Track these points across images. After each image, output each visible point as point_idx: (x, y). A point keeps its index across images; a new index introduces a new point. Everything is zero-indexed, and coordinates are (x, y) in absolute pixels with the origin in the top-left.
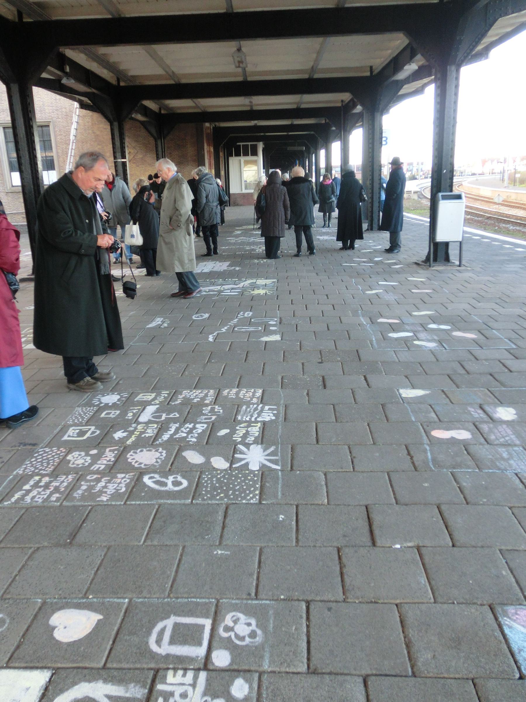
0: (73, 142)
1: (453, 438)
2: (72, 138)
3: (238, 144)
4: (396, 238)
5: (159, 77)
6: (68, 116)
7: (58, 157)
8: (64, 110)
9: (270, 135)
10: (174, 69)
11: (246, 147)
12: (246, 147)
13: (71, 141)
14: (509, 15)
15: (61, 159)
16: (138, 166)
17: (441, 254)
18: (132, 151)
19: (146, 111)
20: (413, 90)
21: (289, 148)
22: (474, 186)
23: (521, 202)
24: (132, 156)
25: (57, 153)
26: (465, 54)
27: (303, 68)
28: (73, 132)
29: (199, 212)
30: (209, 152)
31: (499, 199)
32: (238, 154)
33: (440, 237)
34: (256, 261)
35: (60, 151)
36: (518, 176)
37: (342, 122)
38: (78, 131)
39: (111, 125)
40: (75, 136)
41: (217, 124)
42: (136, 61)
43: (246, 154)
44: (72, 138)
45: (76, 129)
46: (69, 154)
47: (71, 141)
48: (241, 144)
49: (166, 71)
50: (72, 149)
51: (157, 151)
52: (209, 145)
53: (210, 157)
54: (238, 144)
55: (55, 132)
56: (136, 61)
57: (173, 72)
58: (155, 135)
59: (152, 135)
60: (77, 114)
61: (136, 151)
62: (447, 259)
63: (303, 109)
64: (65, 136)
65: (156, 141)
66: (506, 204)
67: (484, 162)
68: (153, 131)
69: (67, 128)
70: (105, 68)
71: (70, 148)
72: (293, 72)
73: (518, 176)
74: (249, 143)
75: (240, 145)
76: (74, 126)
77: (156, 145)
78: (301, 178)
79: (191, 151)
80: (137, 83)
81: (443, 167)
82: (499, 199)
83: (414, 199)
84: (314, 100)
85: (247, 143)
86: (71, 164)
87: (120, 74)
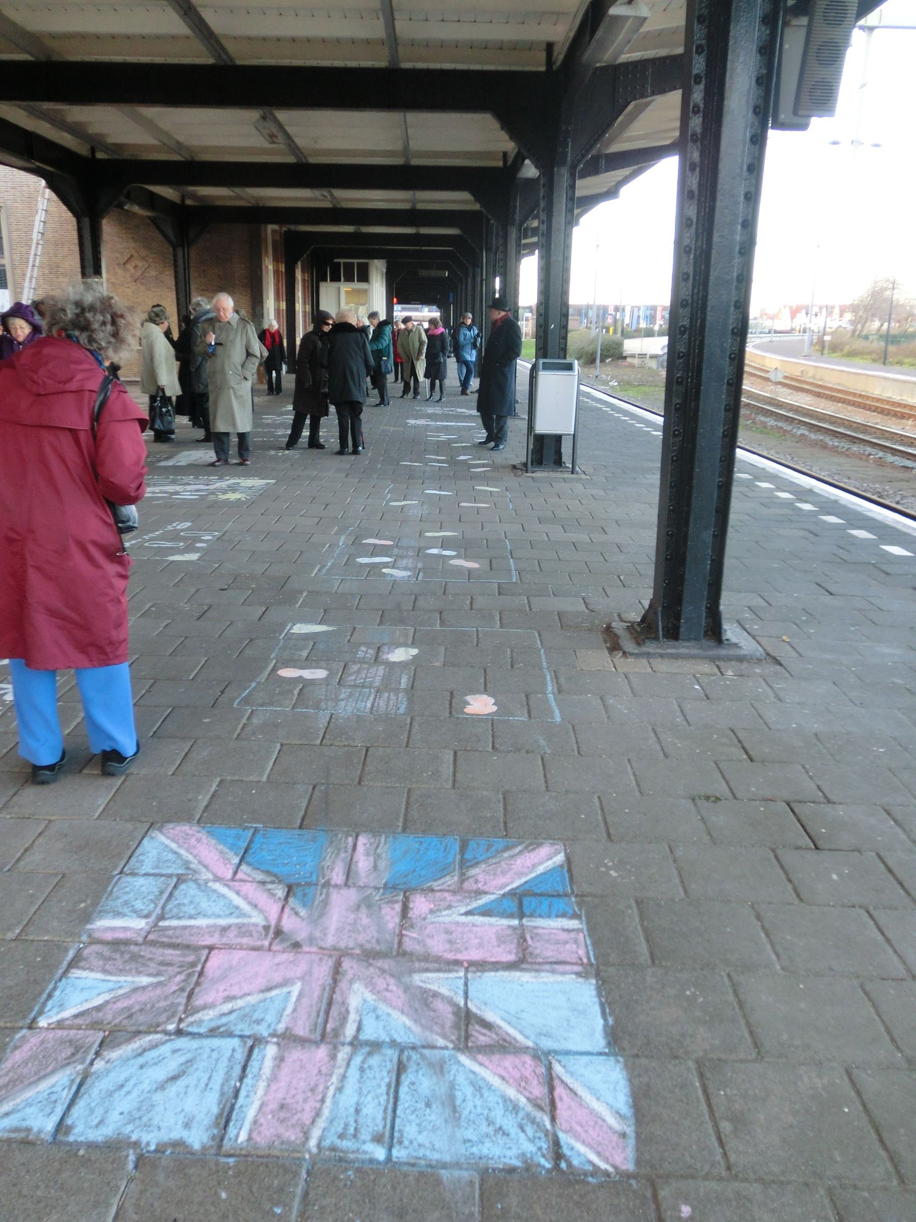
0: (38, 244)
1: (301, 677)
2: (35, 236)
3: (336, 260)
4: (503, 427)
5: (153, 148)
6: (31, 200)
7: (13, 266)
8: (25, 188)
9: (392, 250)
10: (181, 138)
11: (349, 268)
12: (349, 268)
13: (35, 242)
14: (647, 97)
15: (18, 271)
16: (149, 289)
17: (549, 453)
18: (140, 264)
19: (152, 201)
20: (605, 190)
21: (423, 273)
22: (759, 352)
23: (820, 383)
24: (139, 273)
25: (12, 260)
26: (583, 152)
27: (391, 148)
28: (38, 226)
29: (193, 370)
30: (276, 272)
31: (776, 375)
32: (336, 278)
33: (542, 427)
34: (273, 452)
35: (16, 257)
36: (827, 338)
37: (484, 235)
38: (48, 225)
39: (79, 222)
40: (43, 234)
41: (292, 227)
42: (117, 126)
43: (349, 279)
44: (35, 236)
45: (44, 222)
46: (31, 264)
47: (35, 242)
48: (342, 261)
49: (160, 141)
50: (36, 255)
51: (176, 266)
52: (276, 260)
53: (278, 281)
54: (336, 260)
55: (9, 224)
56: (117, 126)
57: (178, 143)
58: (173, 238)
59: (170, 242)
60: (46, 197)
61: (147, 265)
62: (558, 462)
63: (420, 211)
64: (26, 233)
65: (174, 250)
66: (795, 385)
67: (794, 313)
68: (170, 233)
69: (30, 218)
70: (62, 129)
71: (32, 252)
72: (373, 153)
73: (827, 338)
74: (356, 261)
75: (340, 263)
76: (40, 216)
77: (175, 256)
78: (350, 325)
79: (239, 270)
80: (126, 155)
81: (550, 320)
82: (776, 375)
83: (650, 368)
84: (443, 198)
85: (352, 261)
86: (34, 280)
87: (95, 142)
